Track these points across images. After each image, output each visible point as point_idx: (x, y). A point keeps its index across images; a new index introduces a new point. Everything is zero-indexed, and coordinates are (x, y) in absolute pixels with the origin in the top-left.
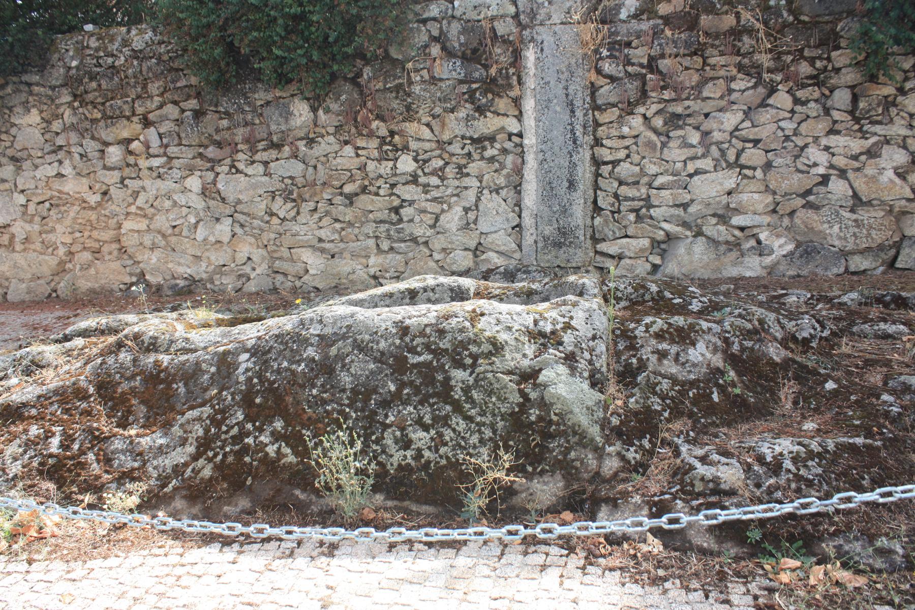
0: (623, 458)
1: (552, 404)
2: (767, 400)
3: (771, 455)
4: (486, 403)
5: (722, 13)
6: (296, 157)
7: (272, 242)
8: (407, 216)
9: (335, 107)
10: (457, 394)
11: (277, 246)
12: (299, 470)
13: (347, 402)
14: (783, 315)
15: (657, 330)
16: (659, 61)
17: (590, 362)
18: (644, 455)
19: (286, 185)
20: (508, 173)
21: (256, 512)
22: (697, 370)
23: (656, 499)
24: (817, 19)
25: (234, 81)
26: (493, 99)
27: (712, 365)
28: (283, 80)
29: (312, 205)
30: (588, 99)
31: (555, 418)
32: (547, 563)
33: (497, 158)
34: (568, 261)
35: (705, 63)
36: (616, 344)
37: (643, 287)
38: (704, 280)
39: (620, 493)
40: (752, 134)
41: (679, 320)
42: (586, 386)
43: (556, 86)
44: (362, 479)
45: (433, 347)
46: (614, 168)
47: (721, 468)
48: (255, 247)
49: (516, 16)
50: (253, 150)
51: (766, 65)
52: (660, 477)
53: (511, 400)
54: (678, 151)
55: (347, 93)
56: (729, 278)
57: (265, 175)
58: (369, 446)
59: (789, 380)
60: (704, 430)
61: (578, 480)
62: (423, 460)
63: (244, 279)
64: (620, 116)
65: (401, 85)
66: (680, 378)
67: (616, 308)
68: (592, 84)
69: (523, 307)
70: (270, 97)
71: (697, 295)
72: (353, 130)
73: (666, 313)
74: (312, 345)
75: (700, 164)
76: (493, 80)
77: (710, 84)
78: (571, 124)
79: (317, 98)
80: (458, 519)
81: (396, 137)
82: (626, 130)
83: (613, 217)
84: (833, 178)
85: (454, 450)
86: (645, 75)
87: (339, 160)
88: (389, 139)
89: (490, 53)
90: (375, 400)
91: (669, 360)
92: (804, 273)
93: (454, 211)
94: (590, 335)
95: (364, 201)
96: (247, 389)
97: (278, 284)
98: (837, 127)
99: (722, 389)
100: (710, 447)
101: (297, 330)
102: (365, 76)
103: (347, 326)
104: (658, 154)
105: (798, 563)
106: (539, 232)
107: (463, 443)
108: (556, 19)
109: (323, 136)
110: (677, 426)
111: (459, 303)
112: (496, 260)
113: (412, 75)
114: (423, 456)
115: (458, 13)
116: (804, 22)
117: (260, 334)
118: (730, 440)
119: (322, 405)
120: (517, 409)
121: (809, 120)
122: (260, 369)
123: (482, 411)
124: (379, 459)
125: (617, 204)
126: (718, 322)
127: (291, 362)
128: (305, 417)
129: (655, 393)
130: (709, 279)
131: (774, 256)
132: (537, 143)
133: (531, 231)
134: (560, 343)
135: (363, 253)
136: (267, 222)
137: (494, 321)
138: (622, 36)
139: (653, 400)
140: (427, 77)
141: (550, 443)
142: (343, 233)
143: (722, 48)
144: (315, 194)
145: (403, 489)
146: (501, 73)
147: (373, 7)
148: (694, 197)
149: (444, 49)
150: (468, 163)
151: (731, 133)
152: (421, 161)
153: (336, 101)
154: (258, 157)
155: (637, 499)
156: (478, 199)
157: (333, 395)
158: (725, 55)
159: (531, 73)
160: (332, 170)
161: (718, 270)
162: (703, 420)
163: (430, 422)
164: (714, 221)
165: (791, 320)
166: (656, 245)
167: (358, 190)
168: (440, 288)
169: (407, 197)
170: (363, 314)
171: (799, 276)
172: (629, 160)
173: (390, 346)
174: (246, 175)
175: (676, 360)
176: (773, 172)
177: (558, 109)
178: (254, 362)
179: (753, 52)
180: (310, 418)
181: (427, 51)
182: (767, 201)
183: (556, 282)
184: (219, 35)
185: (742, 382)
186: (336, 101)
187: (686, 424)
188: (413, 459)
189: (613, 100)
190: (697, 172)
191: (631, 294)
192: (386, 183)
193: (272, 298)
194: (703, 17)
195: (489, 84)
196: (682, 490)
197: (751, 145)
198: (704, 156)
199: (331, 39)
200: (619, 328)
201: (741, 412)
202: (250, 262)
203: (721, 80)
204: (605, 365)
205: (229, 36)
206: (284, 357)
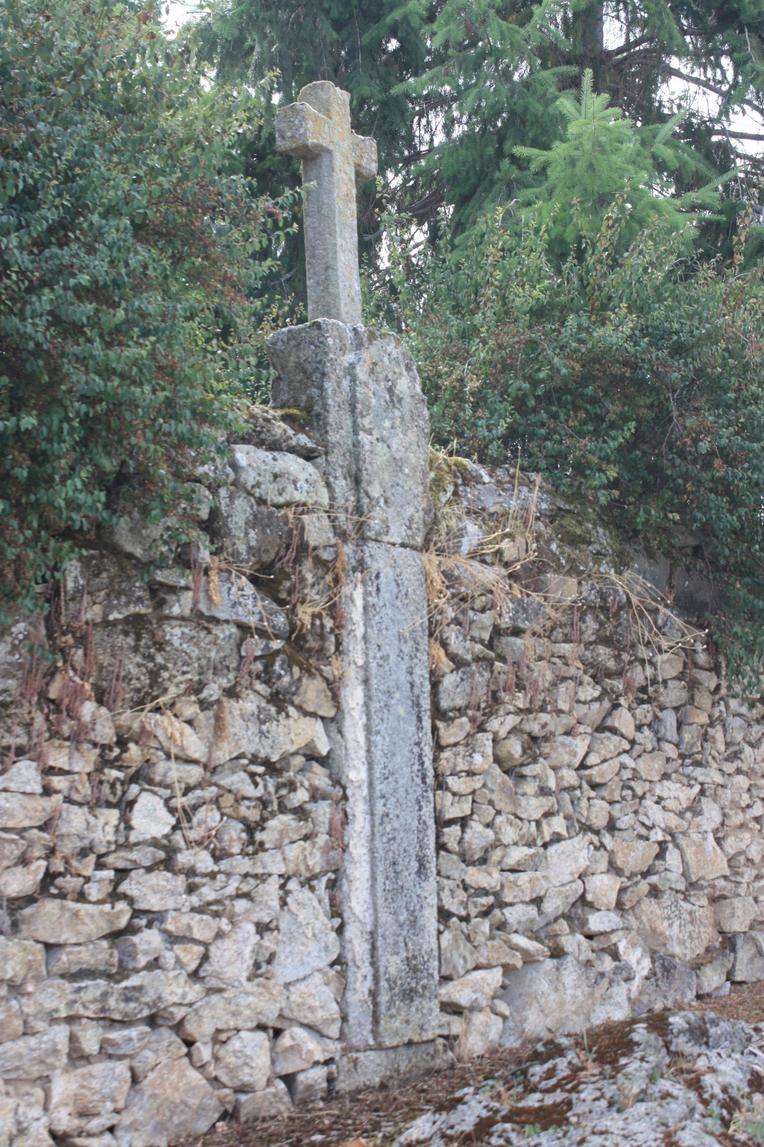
8: (146, 953)
34: (422, 1028)
43: (397, 664)
81: (132, 746)
88: (117, 751)
158: (571, 642)
169: (153, 902)
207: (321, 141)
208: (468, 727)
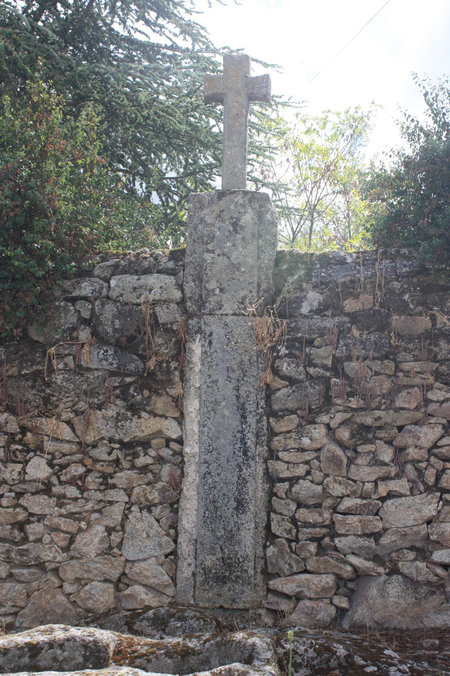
5: (416, 314)
8: (34, 534)
16: (346, 364)
20: (164, 487)
26: (149, 397)
30: (262, 403)
34: (234, 600)
35: (397, 369)
37: (328, 649)
38: (401, 630)
46: (291, 486)
54: (367, 469)
56: (433, 629)
64: (300, 425)
65: (40, 372)
68: (267, 385)
71: (395, 661)
75: (394, 485)
76: (152, 374)
77: (404, 393)
78: (242, 432)
81: (29, 435)
82: (306, 441)
83: (290, 547)
86: (330, 378)
88: (20, 436)
89: (149, 343)
104: (344, 471)
106: (199, 562)
108: (228, 308)
113: (54, 362)
115: (114, 294)
125: (294, 531)
130: (407, 630)
132: (200, 452)
133: (189, 561)
138: (303, 333)
140: (72, 365)
143: (417, 353)
146: (161, 367)
147: (14, 280)
148: (388, 525)
149: (94, 333)
150: (115, 472)
151: (429, 450)
156: (125, 517)
158: (420, 360)
161: (418, 618)
164: (411, 555)
166: (342, 584)
168: (71, 644)
169: (36, 510)
172: (309, 477)
177: (227, 413)
181: (75, 334)
183: (219, 639)
189: (290, 405)
190: (391, 495)
191: (313, 659)
192: (11, 491)
198: (398, 476)
203: (416, 389)
207: (215, 91)
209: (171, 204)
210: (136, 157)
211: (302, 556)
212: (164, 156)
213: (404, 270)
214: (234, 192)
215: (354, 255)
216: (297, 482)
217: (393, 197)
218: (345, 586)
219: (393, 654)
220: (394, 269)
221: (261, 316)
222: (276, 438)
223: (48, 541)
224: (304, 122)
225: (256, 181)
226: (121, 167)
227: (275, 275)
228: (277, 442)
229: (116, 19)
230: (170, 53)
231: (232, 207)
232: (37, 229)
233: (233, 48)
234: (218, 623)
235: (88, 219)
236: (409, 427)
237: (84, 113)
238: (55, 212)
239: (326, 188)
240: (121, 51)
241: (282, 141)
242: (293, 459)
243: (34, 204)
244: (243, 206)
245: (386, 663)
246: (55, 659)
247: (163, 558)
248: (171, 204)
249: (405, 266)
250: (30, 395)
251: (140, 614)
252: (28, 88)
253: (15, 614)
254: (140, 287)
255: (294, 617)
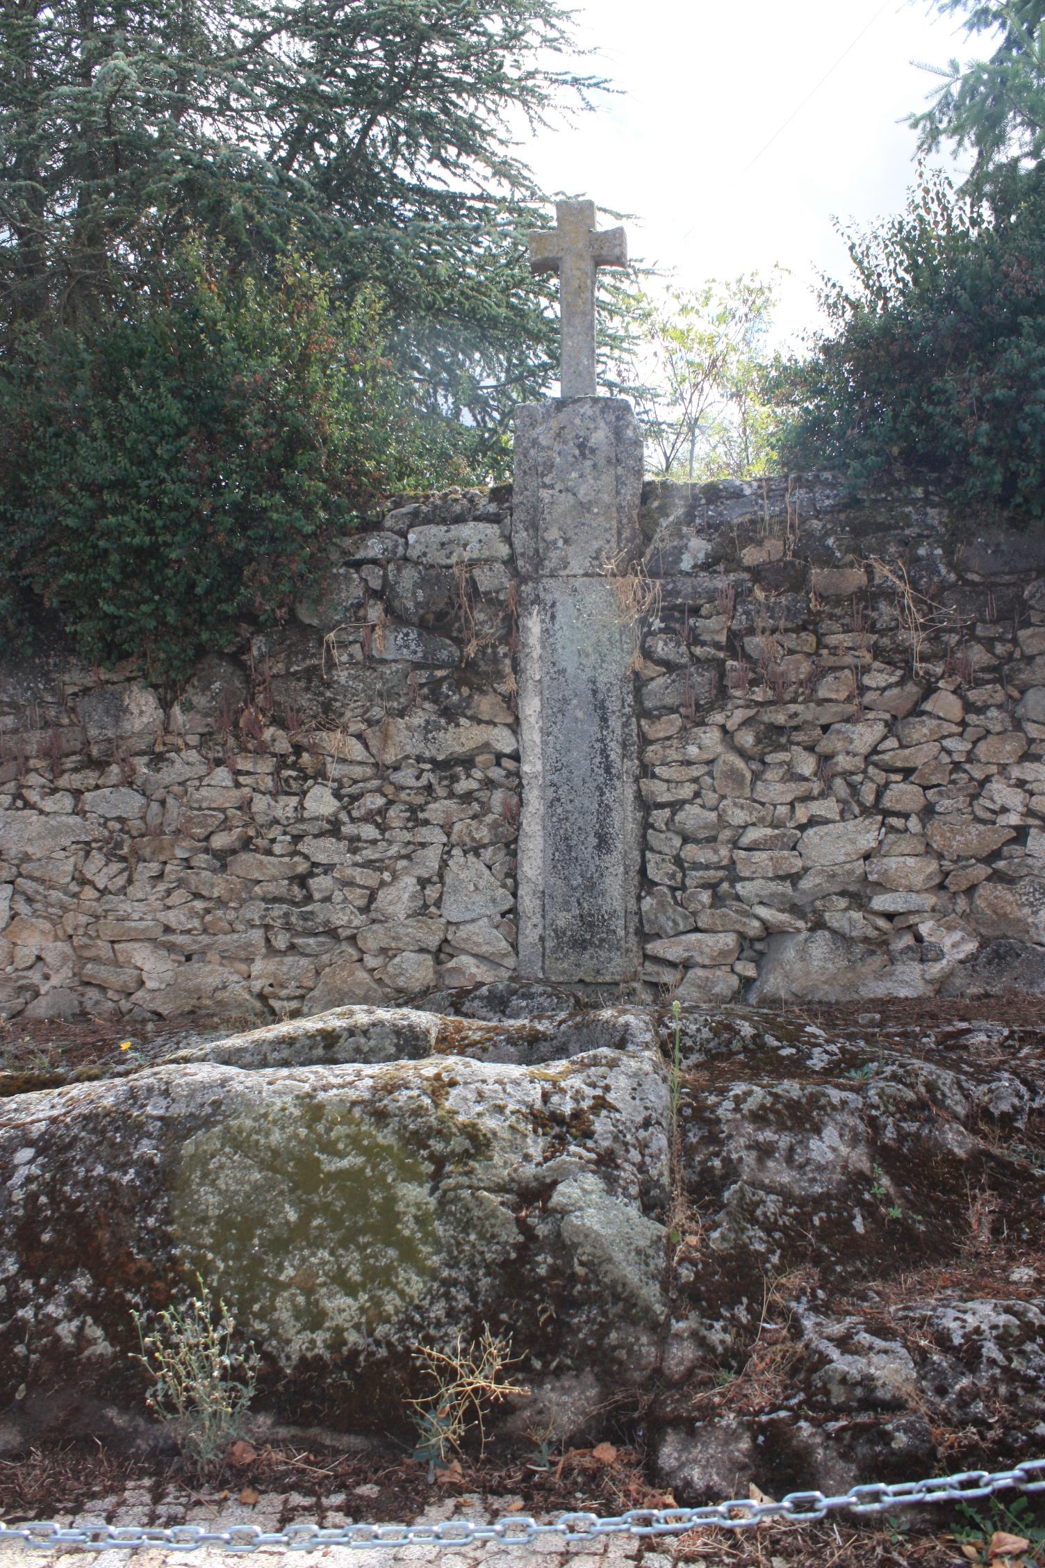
0: (702, 1342)
1: (575, 1246)
2: (946, 1227)
3: (960, 1332)
4: (458, 1244)
5: (845, 565)
6: (131, 784)
7: (81, 931)
8: (320, 891)
9: (201, 701)
10: (407, 1228)
11: (90, 937)
12: (116, 1369)
13: (209, 1241)
14: (966, 1073)
15: (754, 1107)
16: (746, 639)
17: (641, 1168)
18: (738, 1335)
19: (111, 832)
20: (495, 821)
21: (30, 1453)
22: (825, 1176)
23: (764, 1418)
24: (993, 579)
25: (29, 651)
26: (470, 696)
27: (851, 1168)
28: (113, 653)
29: (154, 867)
30: (630, 699)
31: (580, 1271)
32: (572, 1549)
33: (477, 794)
34: (598, 972)
35: (820, 644)
36: (684, 1133)
37: (729, 1028)
38: (829, 1004)
39: (699, 1407)
40: (900, 759)
41: (791, 1088)
42: (633, 1211)
44: (233, 1389)
45: (366, 1143)
46: (674, 814)
47: (875, 1359)
48: (51, 938)
49: (510, 561)
50: (56, 770)
51: (918, 648)
52: (768, 1376)
53: (504, 1238)
54: (779, 787)
55: (222, 679)
56: (872, 1000)
57: (75, 813)
58: (247, 1324)
59: (983, 1190)
60: (838, 1287)
61: (624, 1383)
62: (345, 1350)
63: (28, 995)
64: (684, 728)
65: (315, 668)
66: (797, 1191)
67: (683, 1067)
68: (636, 674)
69: (524, 1069)
70: (89, 680)
71: (821, 1041)
72: (231, 742)
73: (769, 1073)
74: (149, 1136)
75: (817, 808)
76: (472, 664)
77: (830, 678)
78: (602, 740)
79: (172, 685)
80: (408, 1461)
81: (305, 756)
82: (693, 750)
83: (674, 897)
84: (1033, 831)
85: (401, 1330)
86: (724, 661)
87: (204, 792)
88: (293, 758)
89: (467, 620)
90: (260, 1237)
91: (776, 1160)
92: (996, 990)
93: (402, 884)
94: (639, 1119)
95: (247, 863)
96: (27, 1215)
97: (89, 1005)
98: (1035, 749)
99: (870, 1211)
100: (855, 1319)
101: (123, 1108)
102: (255, 652)
103: (214, 1102)
104: (748, 790)
105: (1023, 1543)
106: (548, 922)
107: (417, 1318)
108: (576, 567)
109: (178, 751)
110: (794, 1279)
111: (412, 1063)
112: (471, 968)
113: (335, 652)
114: (345, 1343)
115: (414, 553)
116: (973, 584)
117: (55, 1113)
118: (888, 1304)
119: (164, 1246)
120: (513, 1255)
121: (990, 738)
122: (53, 1178)
123: (452, 1258)
124: (265, 1347)
125: (679, 875)
126: (860, 1089)
127: (110, 1167)
128: (132, 1268)
129: (754, 1221)
130: (837, 1003)
131: (944, 962)
132: (545, 770)
133: (535, 920)
134: (589, 1134)
135: (243, 954)
136: (75, 895)
137: (472, 1096)
138: (685, 597)
139: (751, 1233)
140: (359, 656)
141: (573, 1316)
142: (208, 918)
143: (847, 620)
144: (161, 849)
145: (307, 1405)
146: (484, 653)
147: (273, 540)
148: (809, 863)
149: (389, 610)
150: (427, 803)
151: (866, 758)
152: (348, 800)
153: (203, 691)
154: (63, 781)
155: (730, 1419)
156: (444, 864)
157: (185, 1228)
159: (535, 655)
160: (192, 808)
161: (852, 987)
162: (839, 1268)
163: (358, 1278)
164: (843, 903)
165: (980, 1082)
166: (746, 944)
167: (237, 845)
168: (378, 1029)
169: (321, 858)
170: (241, 1079)
171: (987, 995)
172: (699, 801)
173: (289, 1139)
174: (41, 812)
175: (789, 1159)
176: (936, 821)
177: (580, 714)
178: (43, 1166)
179: (897, 627)
180: (140, 1271)
181: (361, 613)
182: (929, 870)
183: (579, 1019)
184: (8, 574)
185: (904, 1196)
186: (203, 691)
187: (809, 1276)
188: (327, 1347)
189: (669, 701)
190: (813, 822)
191: (708, 1041)
192: (285, 833)
193: (78, 1029)
194: (815, 571)
195: (464, 671)
196: (807, 1402)
197: (899, 777)
198: (823, 795)
199: (199, 590)
200: (689, 1105)
201: (903, 1250)
202: (40, 964)
203: (847, 671)
204: (666, 1173)
205: (25, 577)
206: (98, 1158)
207: (546, 254)
208: (679, 722)
209: (490, 425)
210: (437, 359)
211: (692, 907)
212: (477, 356)
213: (827, 502)
214: (580, 400)
215: (755, 484)
216: (681, 808)
217: (808, 398)
218: (751, 947)
219: (818, 1032)
220: (813, 501)
221: (624, 576)
222: (651, 748)
223: (340, 899)
224: (678, 297)
225: (610, 385)
226: (416, 375)
227: (642, 516)
228: (652, 752)
229: (400, 162)
230: (479, 205)
231: (577, 421)
232: (301, 466)
233: (571, 193)
234: (577, 1001)
235: (373, 449)
236: (837, 726)
237: (359, 299)
238: (325, 441)
239: (712, 392)
240: (408, 206)
241: (645, 327)
242: (675, 777)
243: (296, 431)
244: (593, 419)
245: (808, 1043)
246: (358, 1050)
247: (498, 917)
248: (490, 425)
249: (828, 497)
250: (304, 700)
251: (470, 992)
252: (278, 265)
253: (302, 997)
254: (451, 542)
255: (681, 991)
